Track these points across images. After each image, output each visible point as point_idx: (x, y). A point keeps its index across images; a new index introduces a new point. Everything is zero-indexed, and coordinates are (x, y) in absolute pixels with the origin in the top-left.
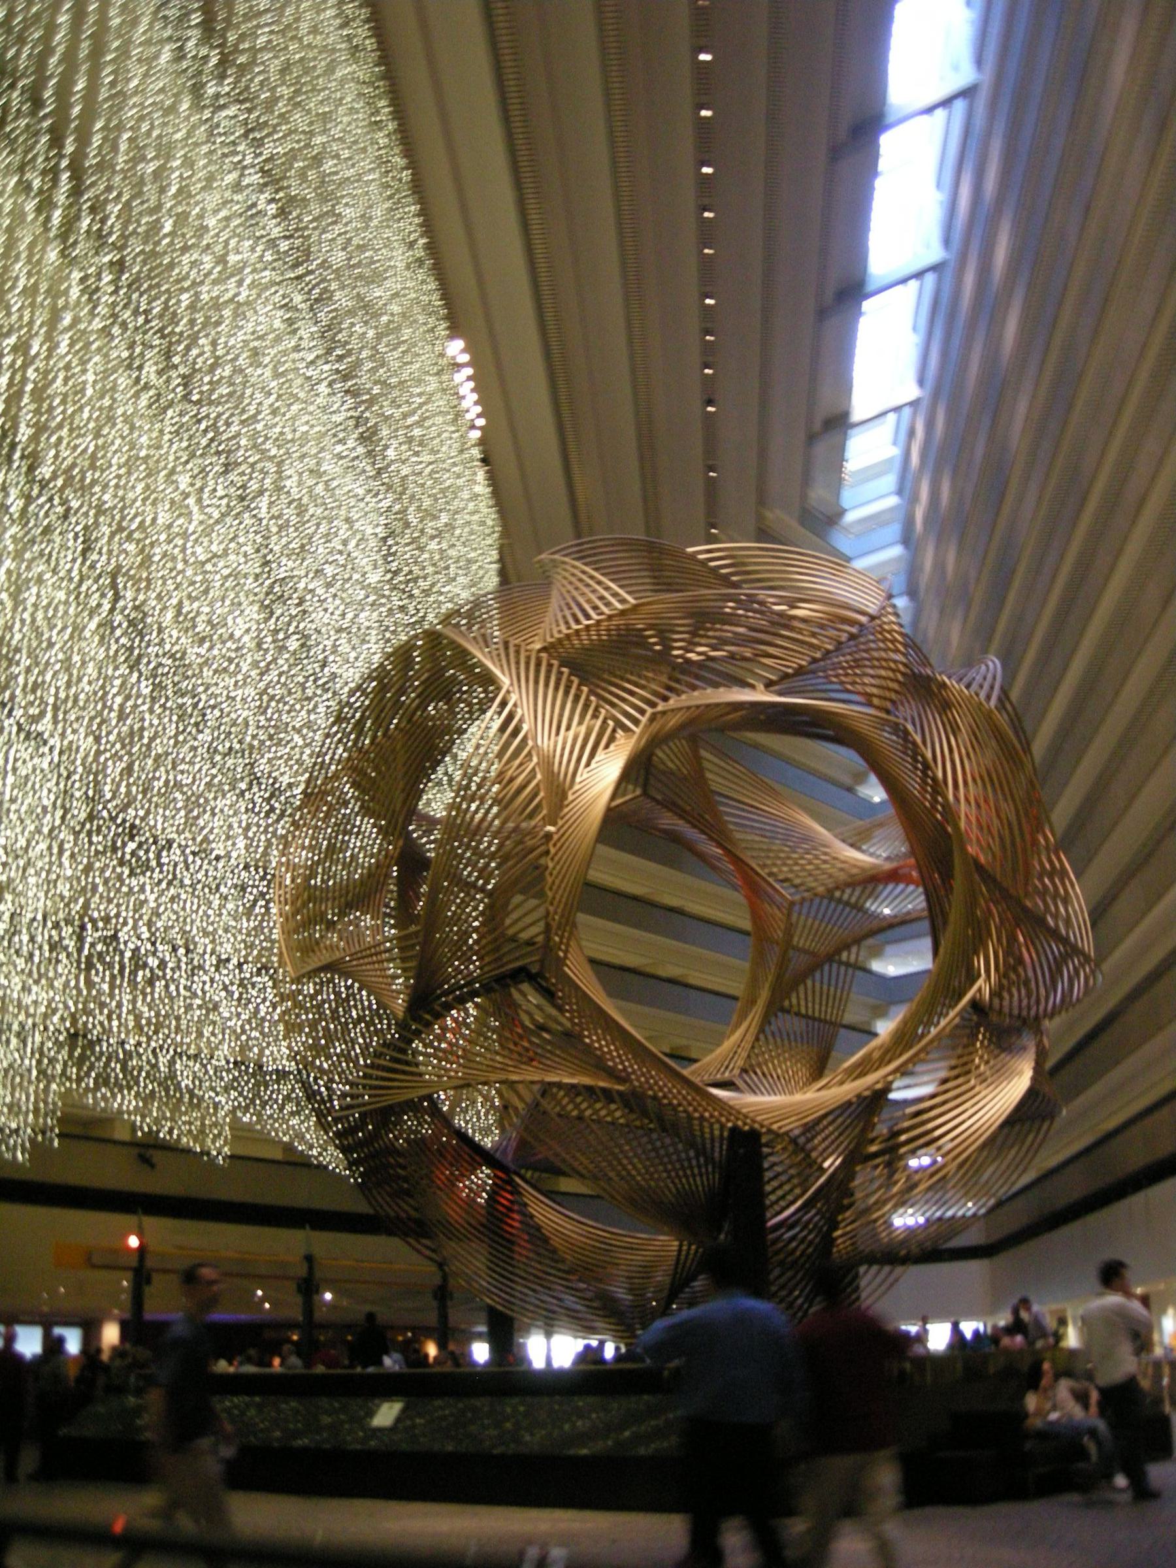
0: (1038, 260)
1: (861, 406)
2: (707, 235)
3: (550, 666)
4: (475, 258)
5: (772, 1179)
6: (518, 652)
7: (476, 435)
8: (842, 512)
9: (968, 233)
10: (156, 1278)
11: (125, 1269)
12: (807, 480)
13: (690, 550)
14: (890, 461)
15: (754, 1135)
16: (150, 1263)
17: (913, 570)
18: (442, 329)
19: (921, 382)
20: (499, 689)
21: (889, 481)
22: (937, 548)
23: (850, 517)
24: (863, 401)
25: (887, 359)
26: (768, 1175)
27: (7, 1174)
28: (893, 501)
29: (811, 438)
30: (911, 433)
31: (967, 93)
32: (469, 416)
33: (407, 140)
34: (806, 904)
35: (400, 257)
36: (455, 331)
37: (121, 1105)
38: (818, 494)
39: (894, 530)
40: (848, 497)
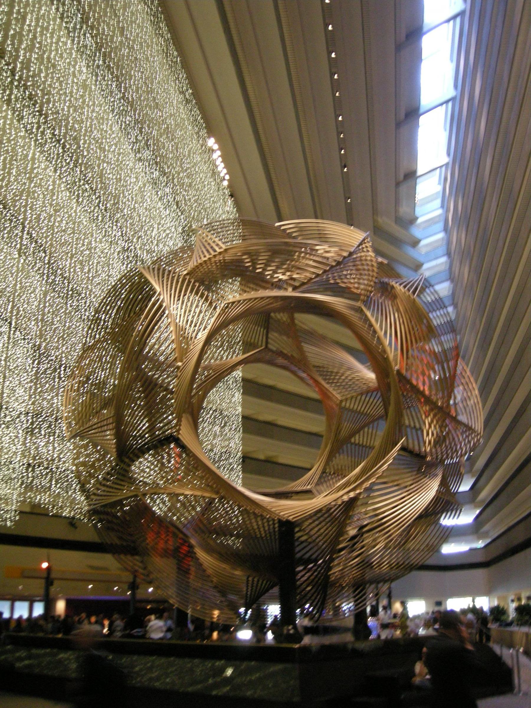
0: (491, 91)
1: (421, 168)
2: (335, 86)
3: (189, 282)
4: (218, 96)
5: (298, 545)
6: (168, 275)
7: (225, 183)
8: (417, 218)
9: (463, 81)
10: (56, 583)
11: (41, 578)
12: (397, 202)
13: (277, 224)
14: (438, 193)
15: (288, 522)
16: (53, 575)
17: (449, 243)
18: (204, 132)
19: (448, 154)
20: (155, 293)
21: (438, 202)
22: (458, 233)
23: (419, 221)
24: (422, 165)
25: (433, 144)
26: (297, 543)
27: (3, 531)
28: (440, 212)
29: (398, 184)
30: (446, 179)
31: (461, 14)
32: (222, 175)
33: (177, 40)
34: (354, 400)
35: (176, 98)
36: (211, 132)
37: (40, 499)
38: (403, 210)
39: (440, 226)
40: (418, 211)
